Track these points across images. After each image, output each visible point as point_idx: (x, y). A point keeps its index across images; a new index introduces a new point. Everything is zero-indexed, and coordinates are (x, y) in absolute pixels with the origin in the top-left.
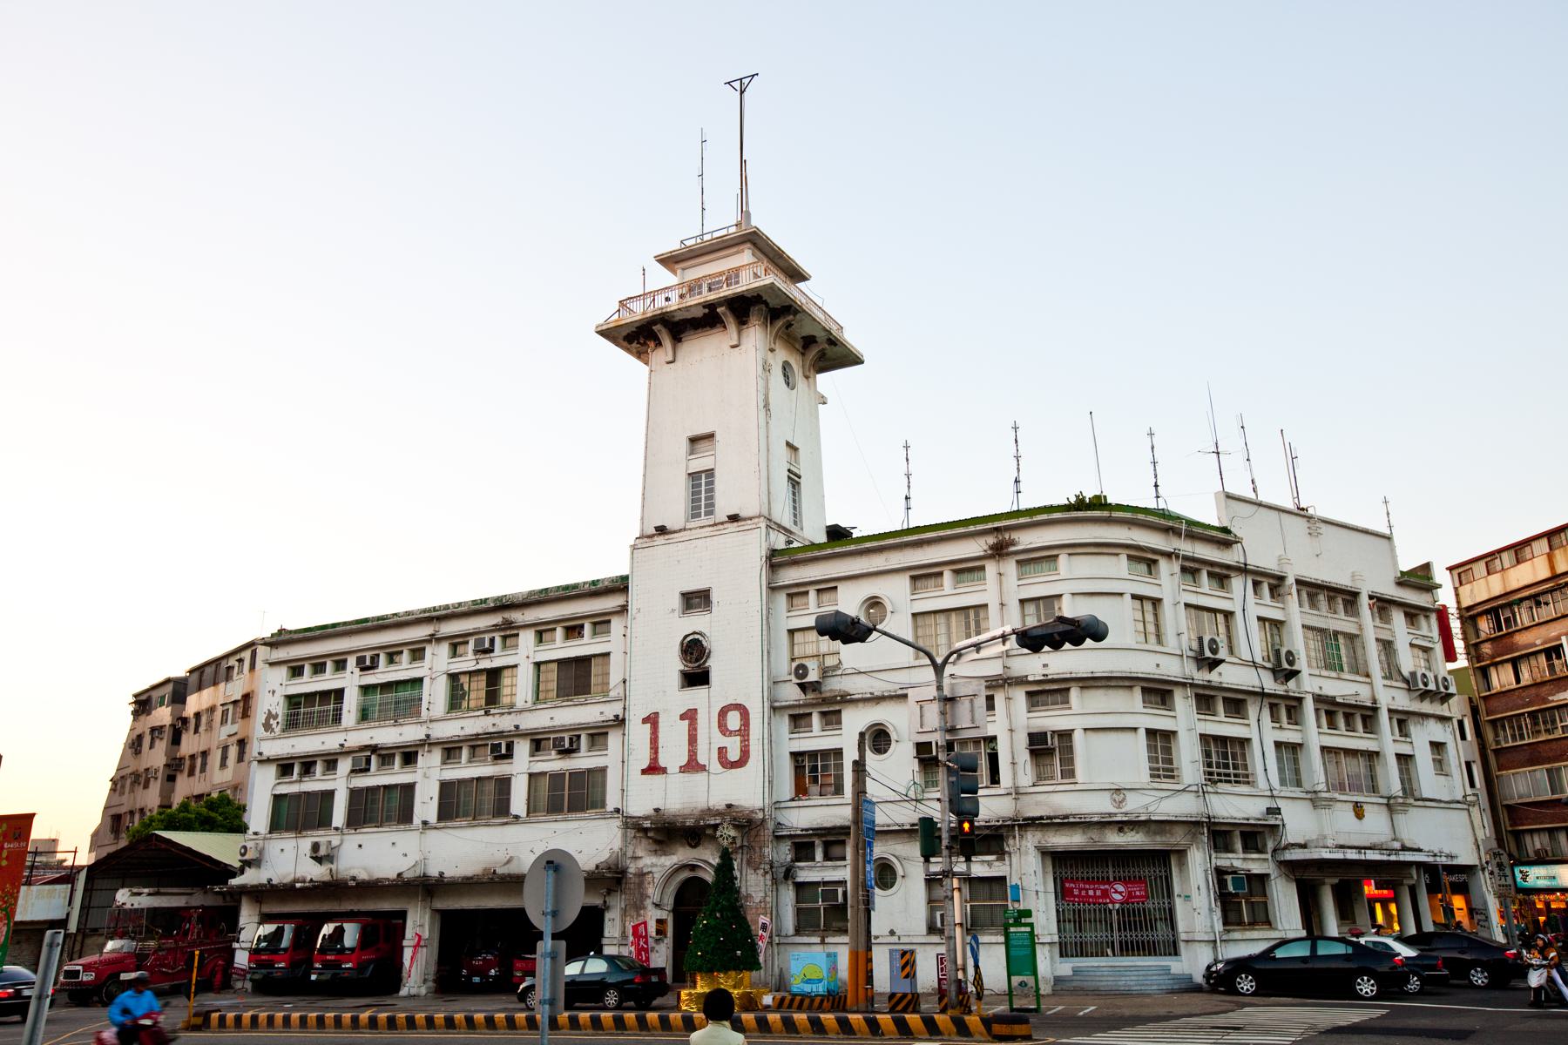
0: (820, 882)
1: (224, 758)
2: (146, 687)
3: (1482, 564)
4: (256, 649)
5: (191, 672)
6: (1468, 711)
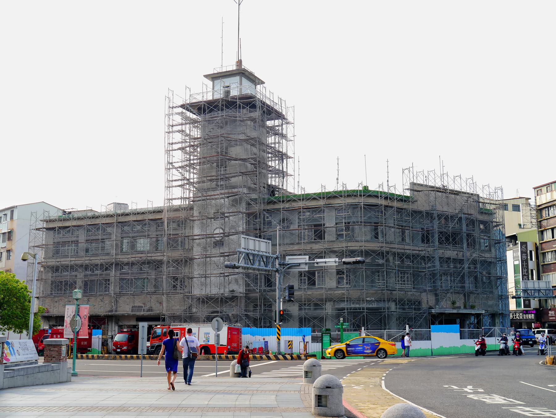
3: (545, 188)
4: (13, 210)
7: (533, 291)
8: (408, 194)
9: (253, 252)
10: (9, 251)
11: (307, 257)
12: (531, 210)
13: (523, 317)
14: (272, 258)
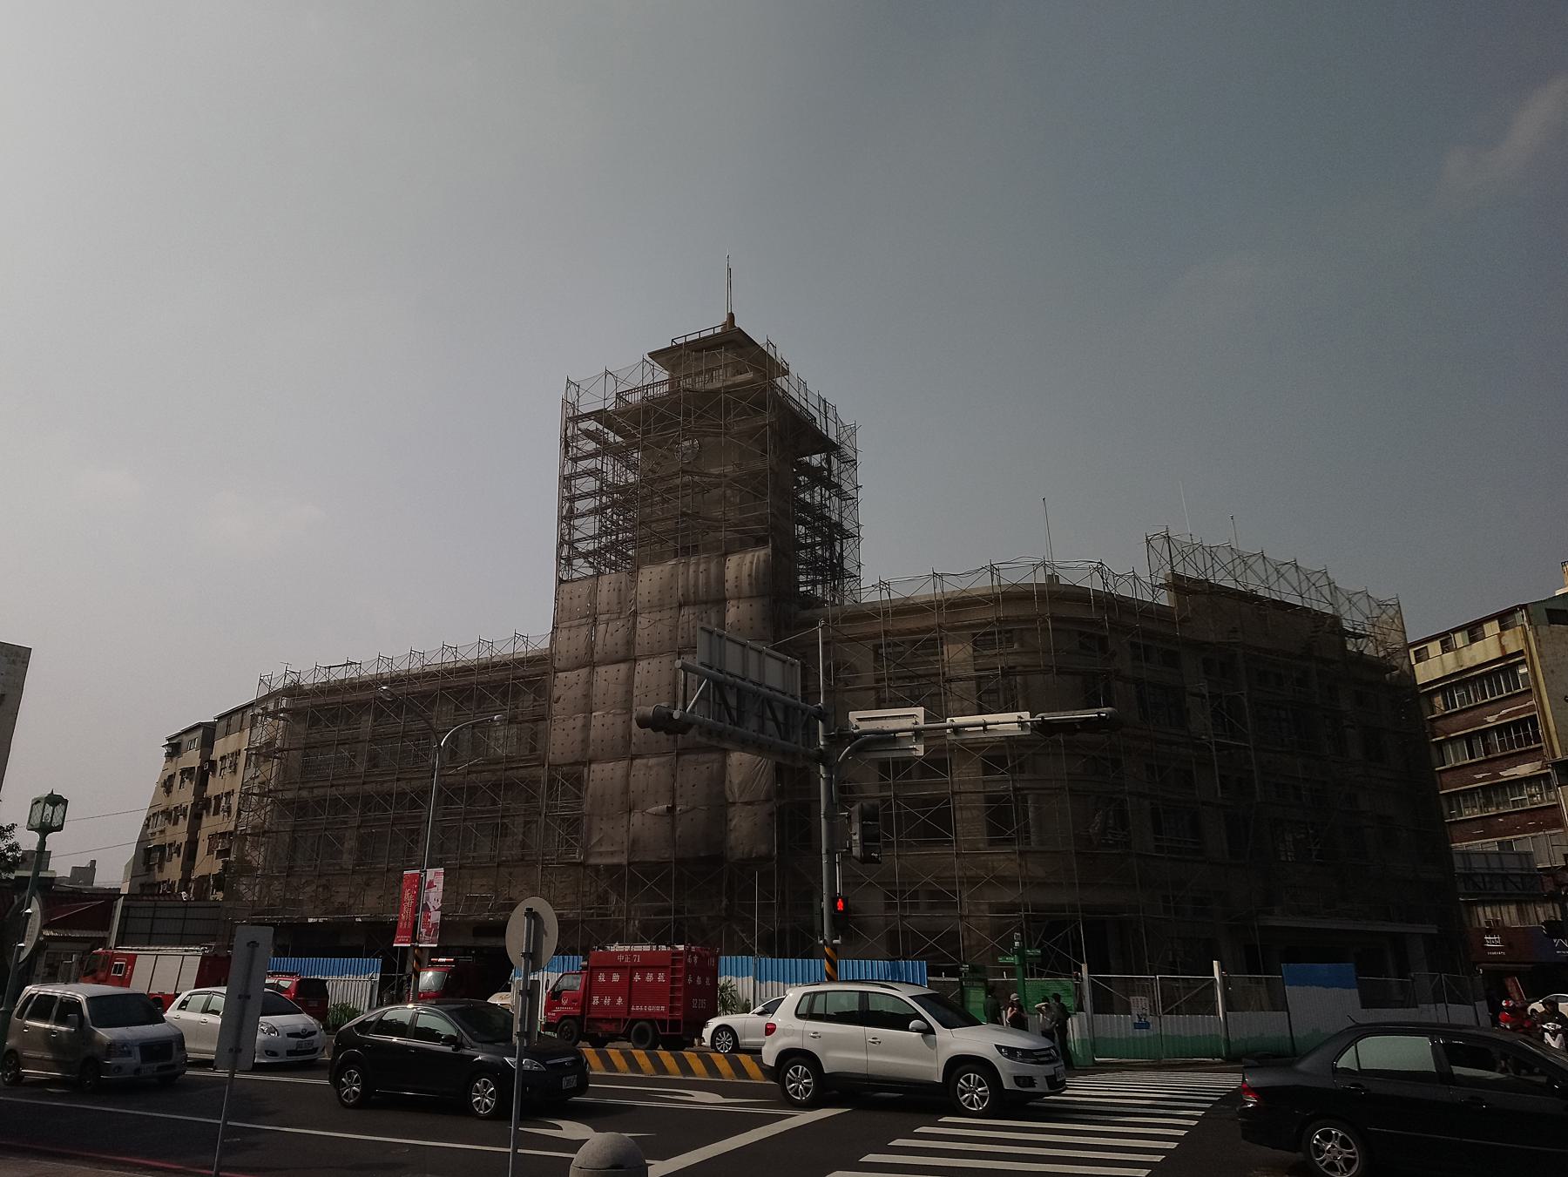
3: (1438, 643)
5: (220, 718)
8: (1164, 599)
11: (920, 711)
14: (803, 713)
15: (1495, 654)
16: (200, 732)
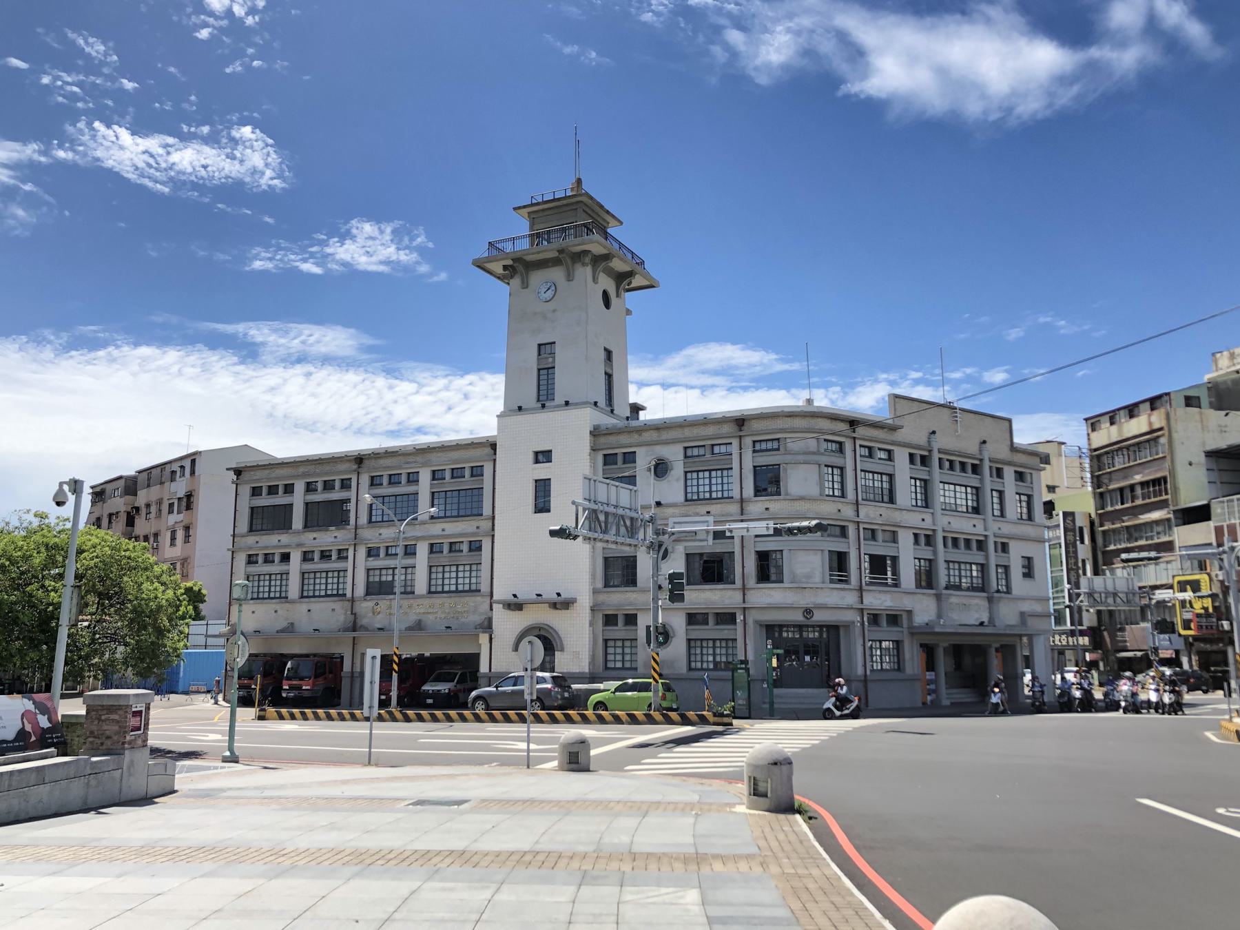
0: (659, 802)
1: (173, 539)
2: (102, 481)
4: (195, 459)
6: (1088, 524)
7: (1103, 595)
9: (607, 509)
10: (187, 528)
12: (1080, 457)
13: (1068, 642)
14: (642, 521)
15: (1145, 429)
16: (122, 482)
